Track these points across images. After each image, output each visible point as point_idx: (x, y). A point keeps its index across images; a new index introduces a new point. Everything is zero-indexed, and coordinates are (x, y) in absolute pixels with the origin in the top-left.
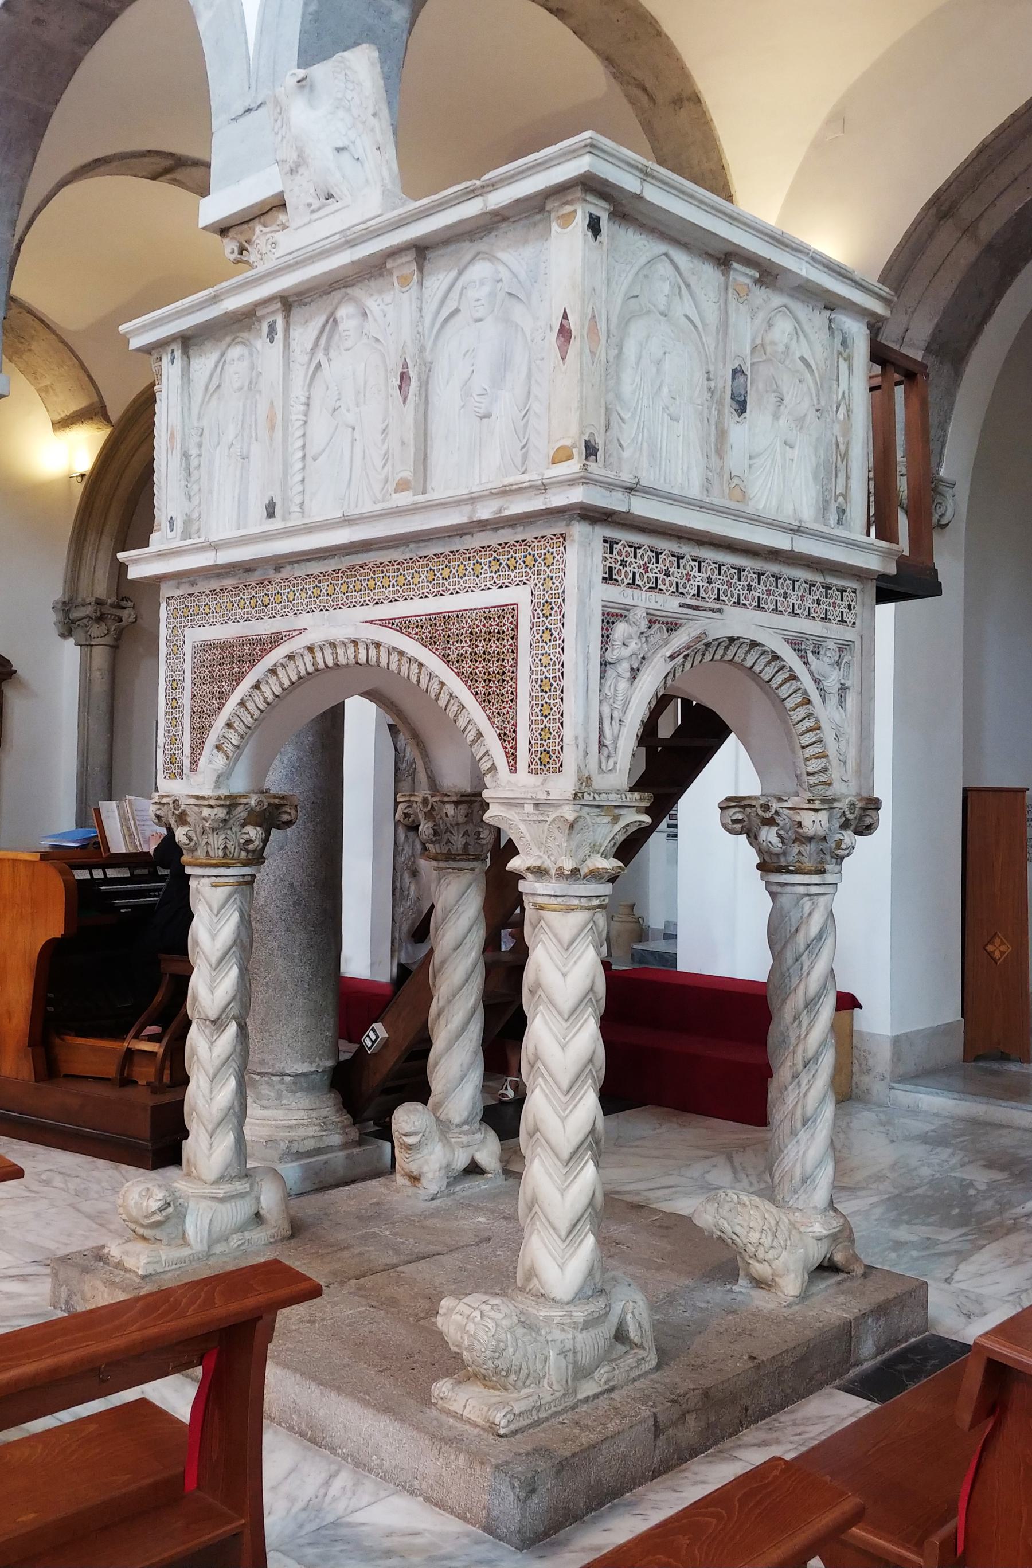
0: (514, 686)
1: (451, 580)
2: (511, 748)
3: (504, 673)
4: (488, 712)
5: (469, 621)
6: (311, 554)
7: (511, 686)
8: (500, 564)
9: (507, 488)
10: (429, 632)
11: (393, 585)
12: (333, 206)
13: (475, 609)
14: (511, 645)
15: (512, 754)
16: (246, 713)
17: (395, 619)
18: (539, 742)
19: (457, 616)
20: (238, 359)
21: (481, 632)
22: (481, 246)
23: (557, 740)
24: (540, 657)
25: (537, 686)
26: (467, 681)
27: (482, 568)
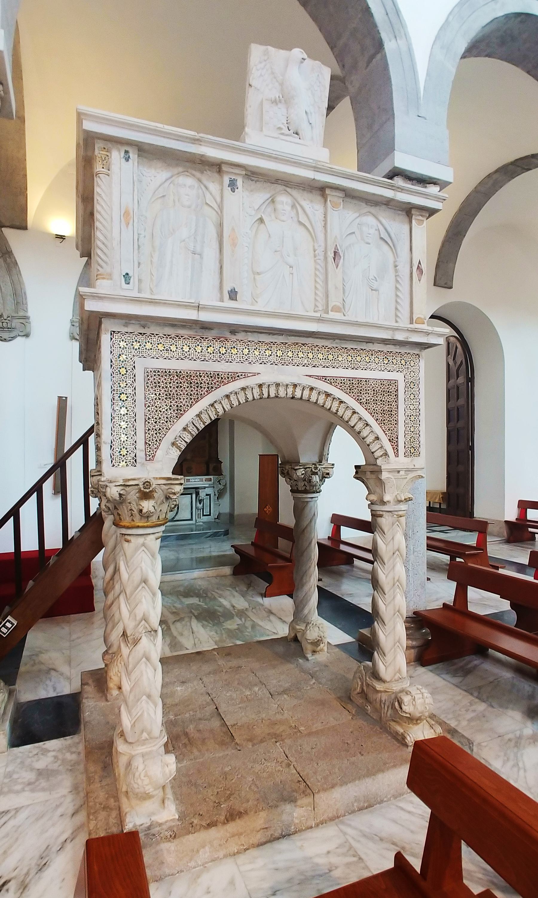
0: (397, 417)
1: (362, 363)
2: (396, 445)
3: (391, 411)
4: (383, 429)
5: (373, 384)
6: (277, 331)
7: (395, 417)
8: (389, 361)
9: (416, 330)
10: (349, 387)
11: (325, 359)
12: (295, 139)
13: (376, 379)
14: (395, 399)
15: (396, 448)
16: (200, 421)
17: (327, 377)
18: (410, 443)
19: (366, 381)
20: (189, 187)
21: (379, 390)
22: (373, 210)
23: (418, 443)
24: (409, 405)
25: (408, 418)
26: (372, 413)
27: (379, 361)
